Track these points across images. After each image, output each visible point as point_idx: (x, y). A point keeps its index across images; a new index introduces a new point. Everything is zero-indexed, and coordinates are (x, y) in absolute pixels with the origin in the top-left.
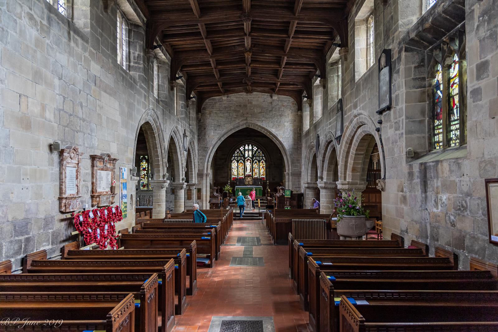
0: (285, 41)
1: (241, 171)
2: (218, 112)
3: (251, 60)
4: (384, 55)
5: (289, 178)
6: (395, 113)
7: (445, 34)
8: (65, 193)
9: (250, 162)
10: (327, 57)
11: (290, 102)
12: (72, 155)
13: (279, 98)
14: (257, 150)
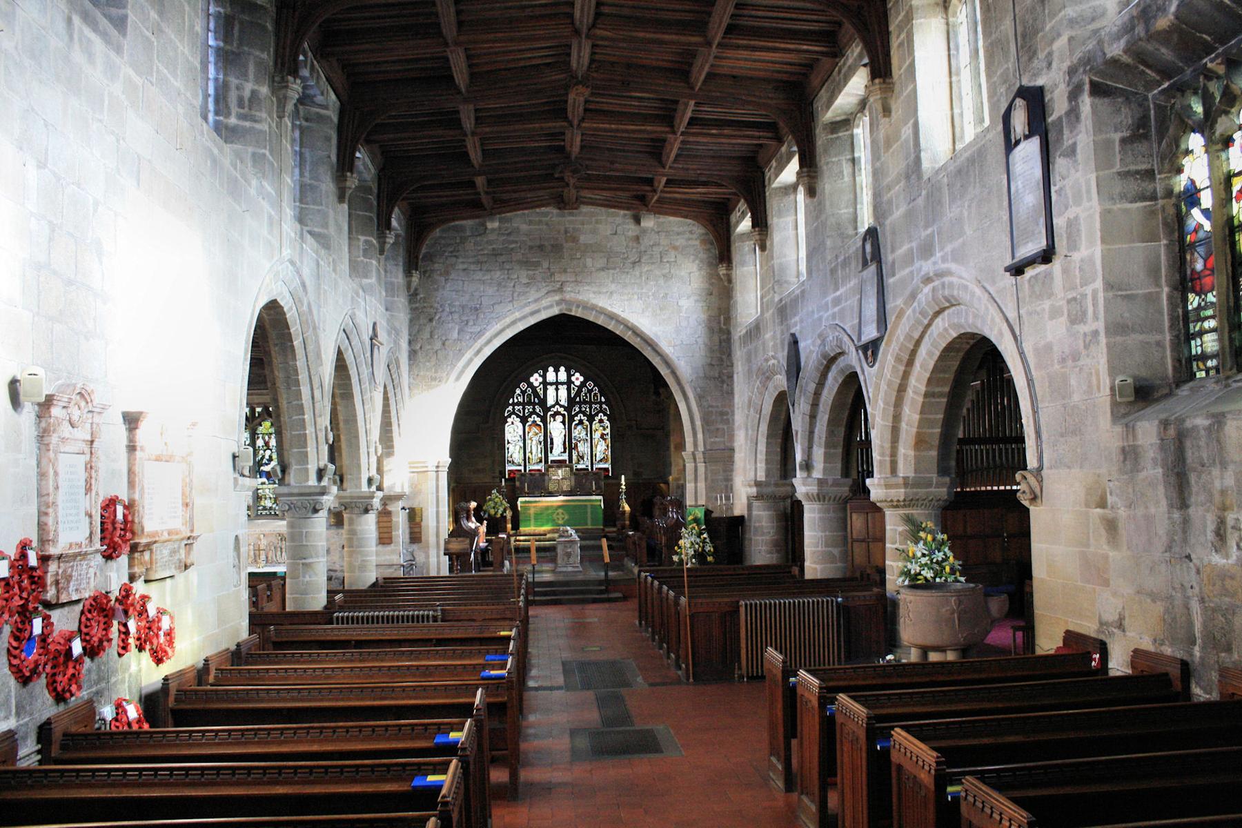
0: (693, 55)
1: (535, 451)
2: (472, 267)
3: (586, 110)
4: (1019, 102)
5: (696, 470)
6: (1065, 271)
7: (1214, 49)
8: (55, 542)
9: (563, 422)
10: (819, 104)
11: (695, 236)
12: (76, 414)
13: (659, 225)
14: (583, 384)
